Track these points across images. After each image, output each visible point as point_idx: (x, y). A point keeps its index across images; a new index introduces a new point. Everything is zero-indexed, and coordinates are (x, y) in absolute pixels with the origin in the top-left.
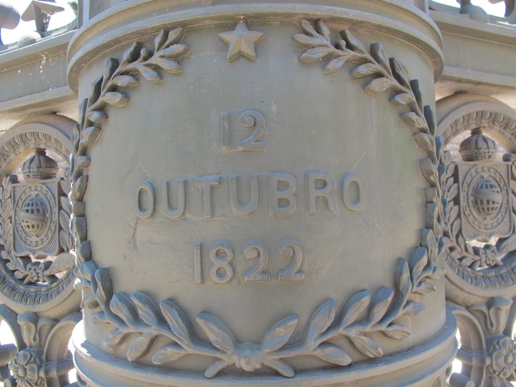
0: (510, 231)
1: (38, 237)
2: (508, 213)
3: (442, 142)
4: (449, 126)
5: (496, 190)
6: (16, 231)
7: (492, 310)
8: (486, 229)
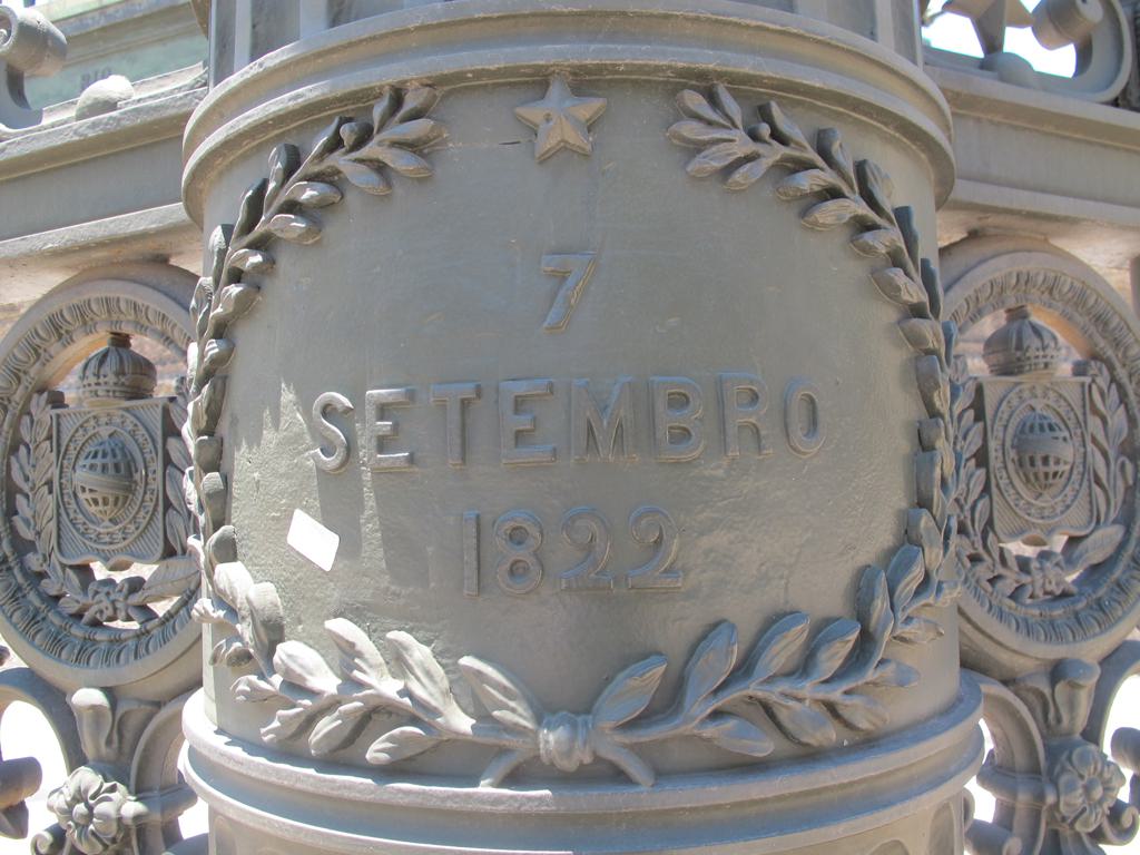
0: (1090, 522)
1: (116, 524)
2: (1085, 483)
5: (1058, 433)
6: (62, 511)
7: (1059, 687)
8: (1043, 518)
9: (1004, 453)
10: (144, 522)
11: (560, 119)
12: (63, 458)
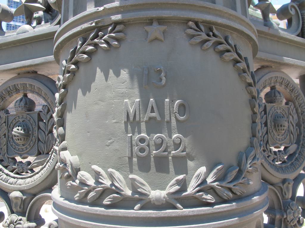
2: (289, 133)
3: (260, 91)
4: (268, 78)
7: (285, 185)
8: (280, 141)
9: (271, 124)
10: (32, 145)
11: (155, 30)
12: (9, 128)
